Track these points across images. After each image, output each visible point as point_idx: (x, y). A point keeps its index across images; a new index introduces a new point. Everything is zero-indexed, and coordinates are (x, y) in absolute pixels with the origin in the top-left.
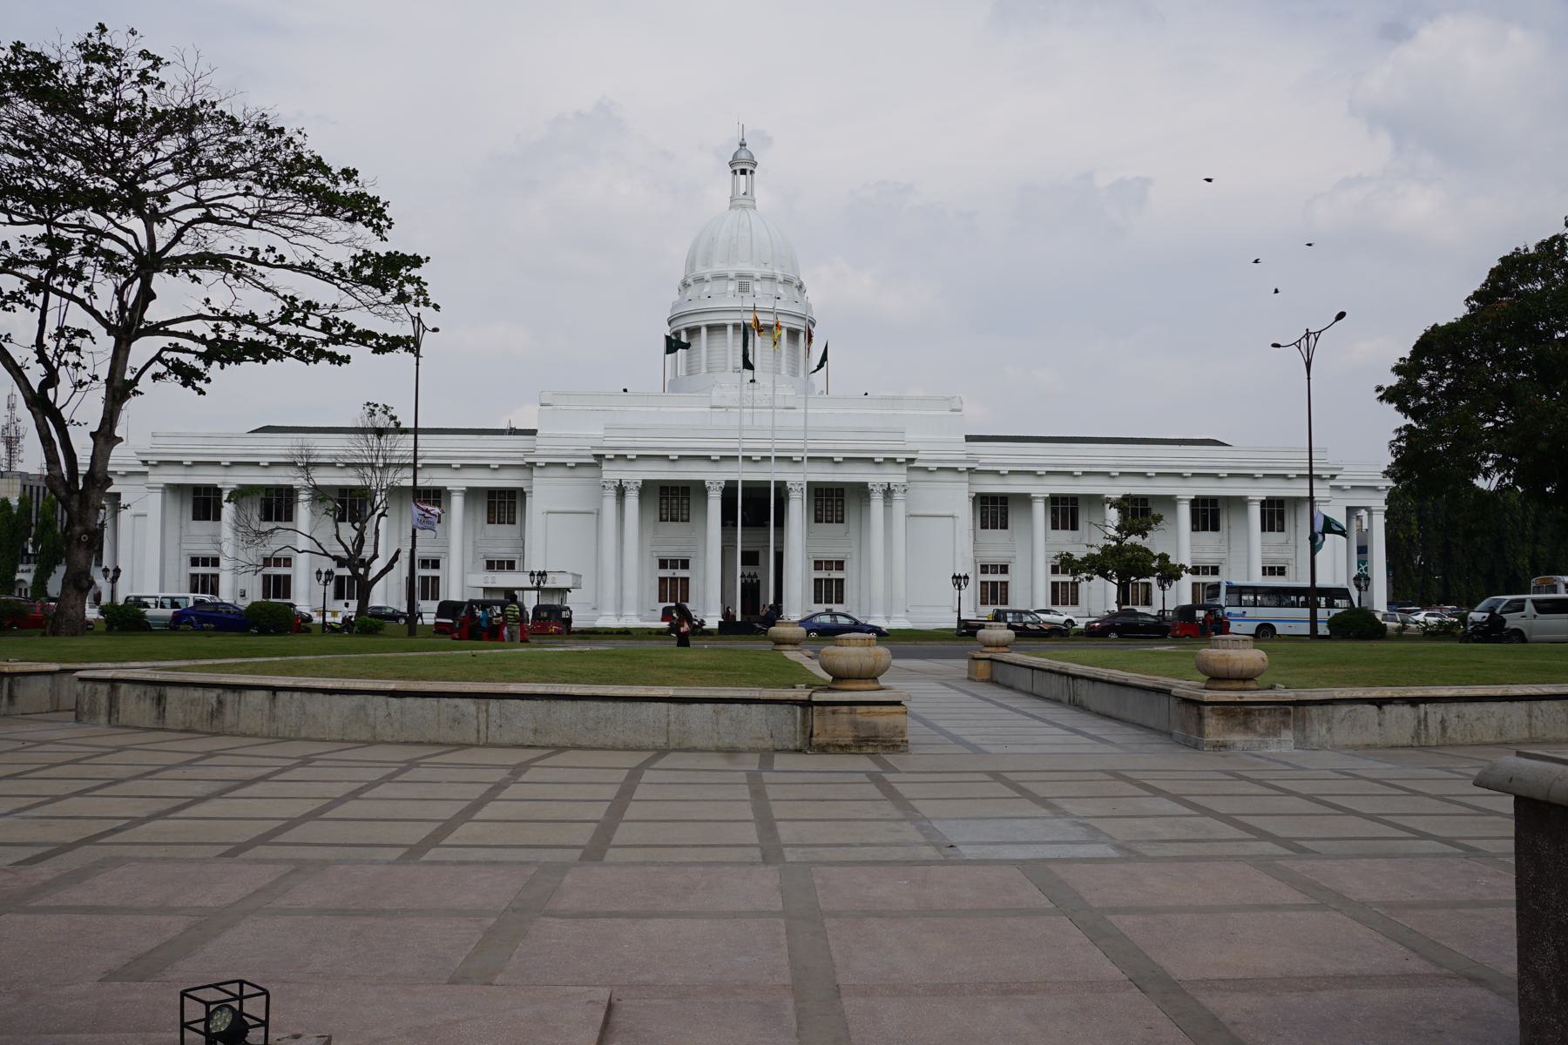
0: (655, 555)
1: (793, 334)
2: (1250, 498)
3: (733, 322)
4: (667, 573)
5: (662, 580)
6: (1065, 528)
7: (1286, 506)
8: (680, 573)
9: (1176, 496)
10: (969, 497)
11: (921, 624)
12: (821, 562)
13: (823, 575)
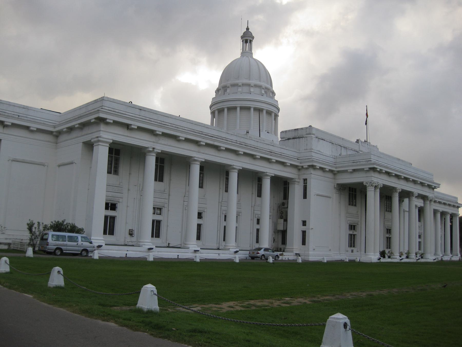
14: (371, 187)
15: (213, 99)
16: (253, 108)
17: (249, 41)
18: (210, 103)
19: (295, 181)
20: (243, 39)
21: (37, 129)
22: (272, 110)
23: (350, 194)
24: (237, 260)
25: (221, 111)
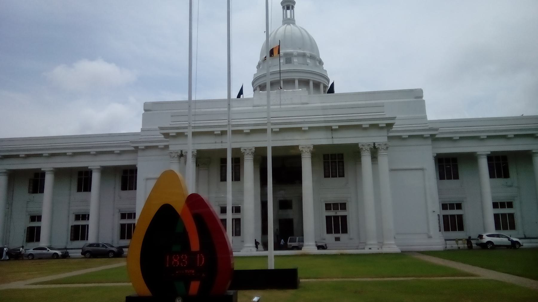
0: (220, 206)
2: (534, 151)
5: (328, 218)
6: (449, 178)
9: (532, 150)
11: (434, 247)
12: (330, 204)
13: (332, 213)
14: (250, 155)
15: (255, 75)
16: (298, 79)
18: (252, 80)
21: (386, 125)
22: (309, 78)
24: (269, 267)
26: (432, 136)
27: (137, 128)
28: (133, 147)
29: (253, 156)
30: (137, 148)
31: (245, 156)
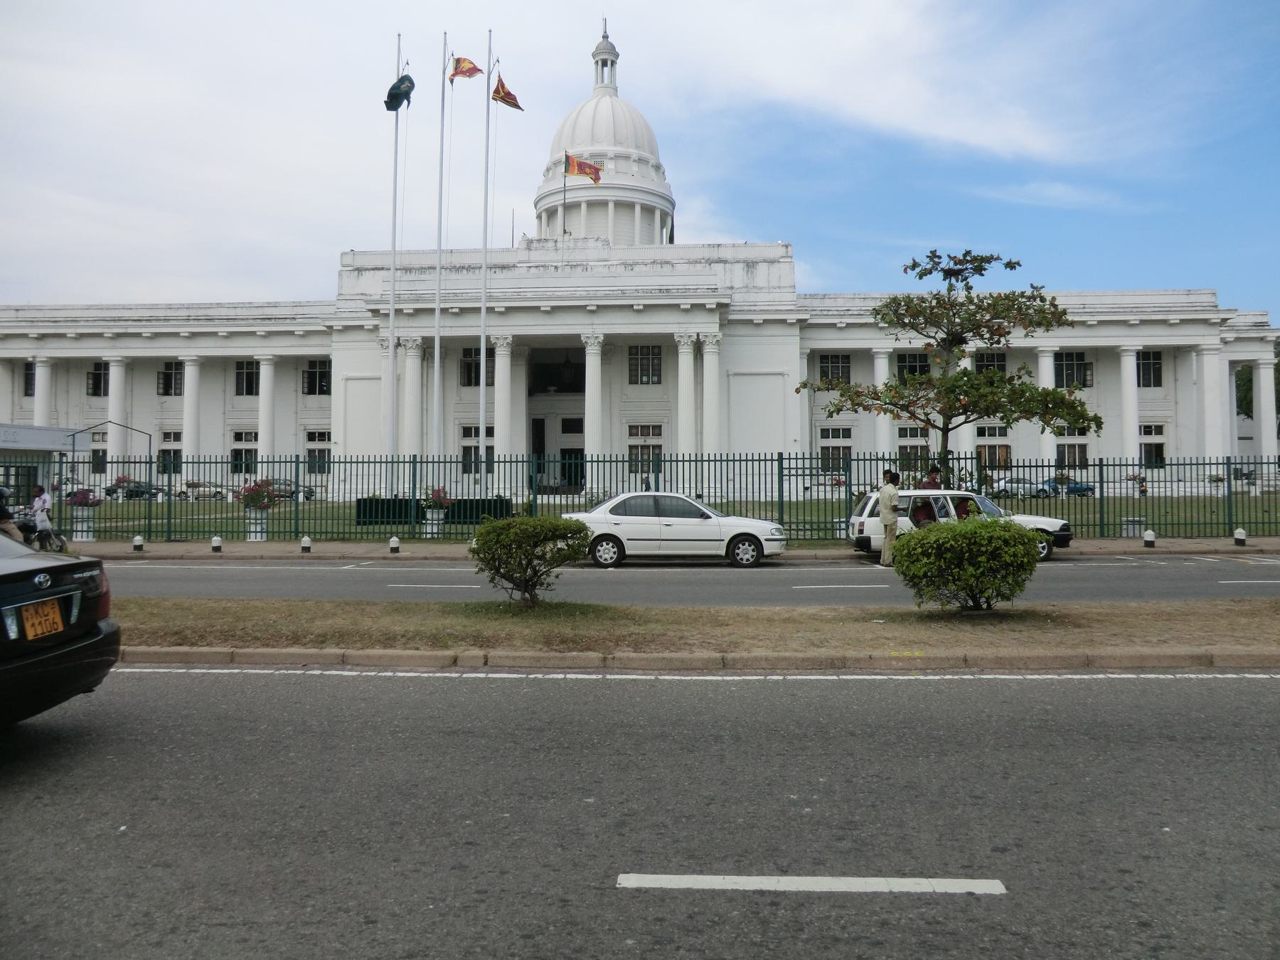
1: (648, 210)
3: (614, 199)
4: (638, 441)
7: (1164, 357)
8: (652, 441)
10: (801, 354)
13: (638, 441)
17: (609, 63)
19: (1259, 364)
20: (596, 59)
23: (238, 374)
25: (551, 213)
26: (799, 321)
27: (331, 295)
28: (1072, 324)
29: (510, 349)
30: (330, 327)
31: (680, 347)
